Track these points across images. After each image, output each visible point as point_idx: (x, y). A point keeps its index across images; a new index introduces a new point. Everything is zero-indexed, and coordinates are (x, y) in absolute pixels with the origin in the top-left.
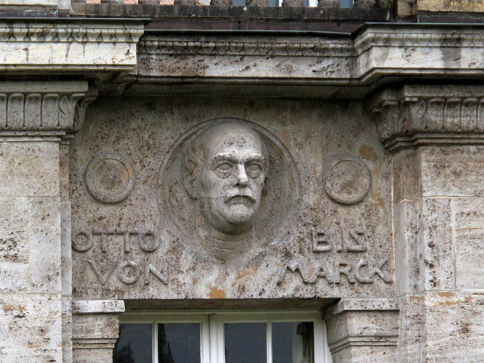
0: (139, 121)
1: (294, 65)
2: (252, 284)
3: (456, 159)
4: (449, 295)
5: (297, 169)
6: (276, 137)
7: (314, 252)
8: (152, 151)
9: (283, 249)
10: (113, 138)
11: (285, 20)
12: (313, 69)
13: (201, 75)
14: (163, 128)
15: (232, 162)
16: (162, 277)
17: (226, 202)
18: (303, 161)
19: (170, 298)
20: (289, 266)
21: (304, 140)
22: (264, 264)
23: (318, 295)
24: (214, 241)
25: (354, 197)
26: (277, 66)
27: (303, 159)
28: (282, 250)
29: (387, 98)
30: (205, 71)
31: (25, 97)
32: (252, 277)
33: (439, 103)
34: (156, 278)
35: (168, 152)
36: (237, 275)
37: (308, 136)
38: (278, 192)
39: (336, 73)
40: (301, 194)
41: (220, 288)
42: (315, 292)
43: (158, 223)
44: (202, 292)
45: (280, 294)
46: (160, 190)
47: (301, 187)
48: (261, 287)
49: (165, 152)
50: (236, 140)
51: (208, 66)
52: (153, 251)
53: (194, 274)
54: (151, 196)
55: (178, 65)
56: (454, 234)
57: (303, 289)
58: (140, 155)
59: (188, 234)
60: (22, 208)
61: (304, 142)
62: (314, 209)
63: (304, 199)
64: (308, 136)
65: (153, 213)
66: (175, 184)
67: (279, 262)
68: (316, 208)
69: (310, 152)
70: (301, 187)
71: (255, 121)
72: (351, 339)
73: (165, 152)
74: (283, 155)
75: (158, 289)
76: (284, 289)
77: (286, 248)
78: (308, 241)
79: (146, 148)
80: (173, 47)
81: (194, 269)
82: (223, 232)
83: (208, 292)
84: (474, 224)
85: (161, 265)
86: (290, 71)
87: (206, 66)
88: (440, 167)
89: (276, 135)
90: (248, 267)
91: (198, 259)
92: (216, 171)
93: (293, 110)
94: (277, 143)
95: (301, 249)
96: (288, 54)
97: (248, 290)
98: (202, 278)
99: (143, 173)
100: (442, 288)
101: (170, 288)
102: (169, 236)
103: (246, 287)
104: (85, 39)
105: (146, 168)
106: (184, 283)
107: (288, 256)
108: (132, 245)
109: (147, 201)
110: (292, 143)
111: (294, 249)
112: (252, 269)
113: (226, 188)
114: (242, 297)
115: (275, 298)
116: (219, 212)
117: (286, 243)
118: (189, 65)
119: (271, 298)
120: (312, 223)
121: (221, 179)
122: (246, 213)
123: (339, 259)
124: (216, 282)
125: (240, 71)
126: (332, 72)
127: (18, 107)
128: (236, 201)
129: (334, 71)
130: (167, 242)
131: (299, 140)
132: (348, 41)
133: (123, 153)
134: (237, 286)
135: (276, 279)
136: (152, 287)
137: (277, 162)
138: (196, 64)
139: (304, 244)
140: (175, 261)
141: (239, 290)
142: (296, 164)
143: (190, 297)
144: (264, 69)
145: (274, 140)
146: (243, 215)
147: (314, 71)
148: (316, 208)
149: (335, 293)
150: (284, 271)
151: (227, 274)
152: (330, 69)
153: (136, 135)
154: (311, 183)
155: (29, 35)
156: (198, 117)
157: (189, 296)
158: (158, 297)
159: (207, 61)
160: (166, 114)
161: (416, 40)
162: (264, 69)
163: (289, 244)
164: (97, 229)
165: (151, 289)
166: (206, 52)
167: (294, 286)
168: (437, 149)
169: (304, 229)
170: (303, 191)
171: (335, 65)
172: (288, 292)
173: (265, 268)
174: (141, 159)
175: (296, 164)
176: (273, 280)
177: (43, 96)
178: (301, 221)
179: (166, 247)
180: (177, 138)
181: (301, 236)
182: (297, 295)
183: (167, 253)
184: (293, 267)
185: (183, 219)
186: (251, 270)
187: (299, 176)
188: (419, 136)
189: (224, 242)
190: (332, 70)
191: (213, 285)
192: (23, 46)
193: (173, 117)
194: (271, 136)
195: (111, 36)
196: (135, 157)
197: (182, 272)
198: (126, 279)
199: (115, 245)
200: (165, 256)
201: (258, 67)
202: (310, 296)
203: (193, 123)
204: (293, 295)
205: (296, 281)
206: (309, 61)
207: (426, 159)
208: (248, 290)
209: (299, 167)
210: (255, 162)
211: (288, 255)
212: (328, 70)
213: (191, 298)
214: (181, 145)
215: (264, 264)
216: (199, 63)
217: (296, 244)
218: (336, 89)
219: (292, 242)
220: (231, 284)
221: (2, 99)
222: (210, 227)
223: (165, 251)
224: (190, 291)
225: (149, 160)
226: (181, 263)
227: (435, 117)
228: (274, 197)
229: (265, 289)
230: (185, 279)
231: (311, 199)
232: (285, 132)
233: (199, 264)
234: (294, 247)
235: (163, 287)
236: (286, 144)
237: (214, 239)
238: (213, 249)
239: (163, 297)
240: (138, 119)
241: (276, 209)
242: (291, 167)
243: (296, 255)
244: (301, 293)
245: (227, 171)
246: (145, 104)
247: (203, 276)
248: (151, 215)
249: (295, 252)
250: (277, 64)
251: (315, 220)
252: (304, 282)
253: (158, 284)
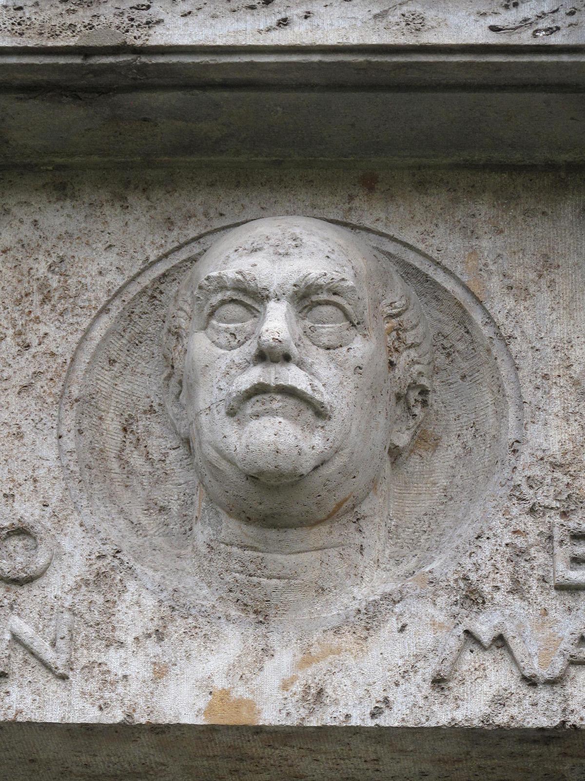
0: (23, 228)
1: (430, 14)
2: (349, 683)
5: (510, 356)
6: (445, 270)
7: (561, 588)
8: (54, 306)
9: (456, 580)
12: (492, 23)
13: (138, 43)
14: (94, 246)
15: (250, 297)
16: (49, 655)
17: (232, 413)
18: (530, 332)
19: (75, 718)
20: (472, 629)
21: (532, 276)
22: (393, 624)
23: (573, 719)
24: (229, 554)
26: (376, 17)
27: (529, 327)
28: (452, 583)
30: (151, 32)
32: (350, 661)
34: (33, 661)
35: (105, 310)
36: (300, 656)
38: (468, 435)
39: (563, 31)
40: (522, 426)
41: (240, 692)
42: (564, 710)
43: (54, 502)
45: (442, 715)
46: (72, 414)
47: (521, 404)
48: (378, 693)
49: (95, 308)
50: (272, 242)
51: (163, 21)
52: (30, 580)
53: (159, 650)
54: (39, 426)
55: (69, 19)
57: (520, 701)
58: (16, 315)
59: (166, 546)
61: (533, 281)
62: (561, 466)
63: (529, 437)
65: (42, 472)
66: (145, 412)
67: (441, 617)
68: (570, 464)
69: (553, 309)
70: (521, 404)
71: (380, 227)
73: (95, 308)
74: (470, 319)
75: (37, 692)
76: (456, 699)
77: (465, 579)
78: (542, 558)
79: (37, 298)
81: (160, 635)
82: (248, 520)
83: (202, 704)
85: (53, 622)
86: (418, 30)
87: (154, 20)
89: (445, 262)
90: (337, 631)
91: (175, 606)
92: (209, 330)
93: (505, 198)
94: (449, 285)
95: (516, 581)
97: (336, 702)
98: (182, 663)
99: (23, 364)
101: (76, 690)
102: (87, 540)
103: (329, 691)
105: (33, 350)
106: (125, 677)
107: (475, 602)
109: (25, 440)
110: (495, 284)
111: (494, 580)
112: (350, 637)
113: (233, 372)
114: (314, 722)
115: (426, 725)
116: (219, 451)
117: (468, 563)
118: (102, 18)
119: (410, 724)
120: (554, 504)
121: (222, 351)
122: (291, 441)
124: (228, 675)
125: (260, 32)
126: (550, 31)
128: (258, 408)
129: (558, 28)
130: (77, 557)
131: (518, 274)
134: (297, 688)
135: (428, 670)
136: (20, 686)
137: (460, 346)
138: (127, 15)
139: (528, 565)
140: (102, 613)
141: (304, 699)
142: (506, 340)
143: (141, 718)
144: (336, 24)
145: (440, 277)
146: (281, 447)
147: (494, 29)
148: (570, 464)
150: (454, 643)
151: (267, 652)
152: (545, 24)
153: (9, 265)
154: (553, 391)
156: (202, 217)
157: (136, 716)
158: (37, 717)
160: (107, 210)
163: (477, 567)
165: (14, 690)
167: (493, 691)
169: (529, 524)
170: (529, 411)
171: (562, 12)
173: (397, 635)
174: (19, 327)
175: (506, 340)
176: (421, 671)
178: (519, 499)
179: (76, 571)
180: (135, 271)
181: (520, 542)
182: (501, 719)
183: (78, 587)
184: (484, 629)
185: (162, 509)
186: (347, 640)
187: (516, 375)
189: (256, 554)
190: (553, 26)
191: (220, 683)
193: (128, 217)
194: (432, 268)
197: (121, 644)
200: (69, 597)
201: (315, 20)
202: (545, 722)
203: (186, 232)
204: (486, 719)
205: (499, 676)
208: (336, 702)
209: (514, 347)
210: (324, 297)
211: (473, 598)
212: (540, 26)
213: (143, 721)
214: (153, 294)
215: (393, 624)
216: (136, 14)
217: (499, 565)
219: (488, 562)
220: (277, 683)
222: (217, 513)
223: (71, 581)
224: (141, 701)
225: (43, 329)
226: (120, 616)
228: (459, 451)
229: (391, 699)
230: (130, 664)
232: (474, 253)
233: (179, 621)
234: (492, 576)
235: (54, 686)
236: (476, 290)
237: (229, 548)
238: (228, 578)
239: (53, 715)
240: (21, 222)
241: (460, 483)
242: (494, 352)
243: (498, 597)
244: (514, 711)
245: (239, 325)
246: (44, 186)
247: (188, 658)
248: (35, 481)
249: (497, 588)
250: (376, 11)
251: (564, 497)
252: (524, 679)
253: (41, 675)
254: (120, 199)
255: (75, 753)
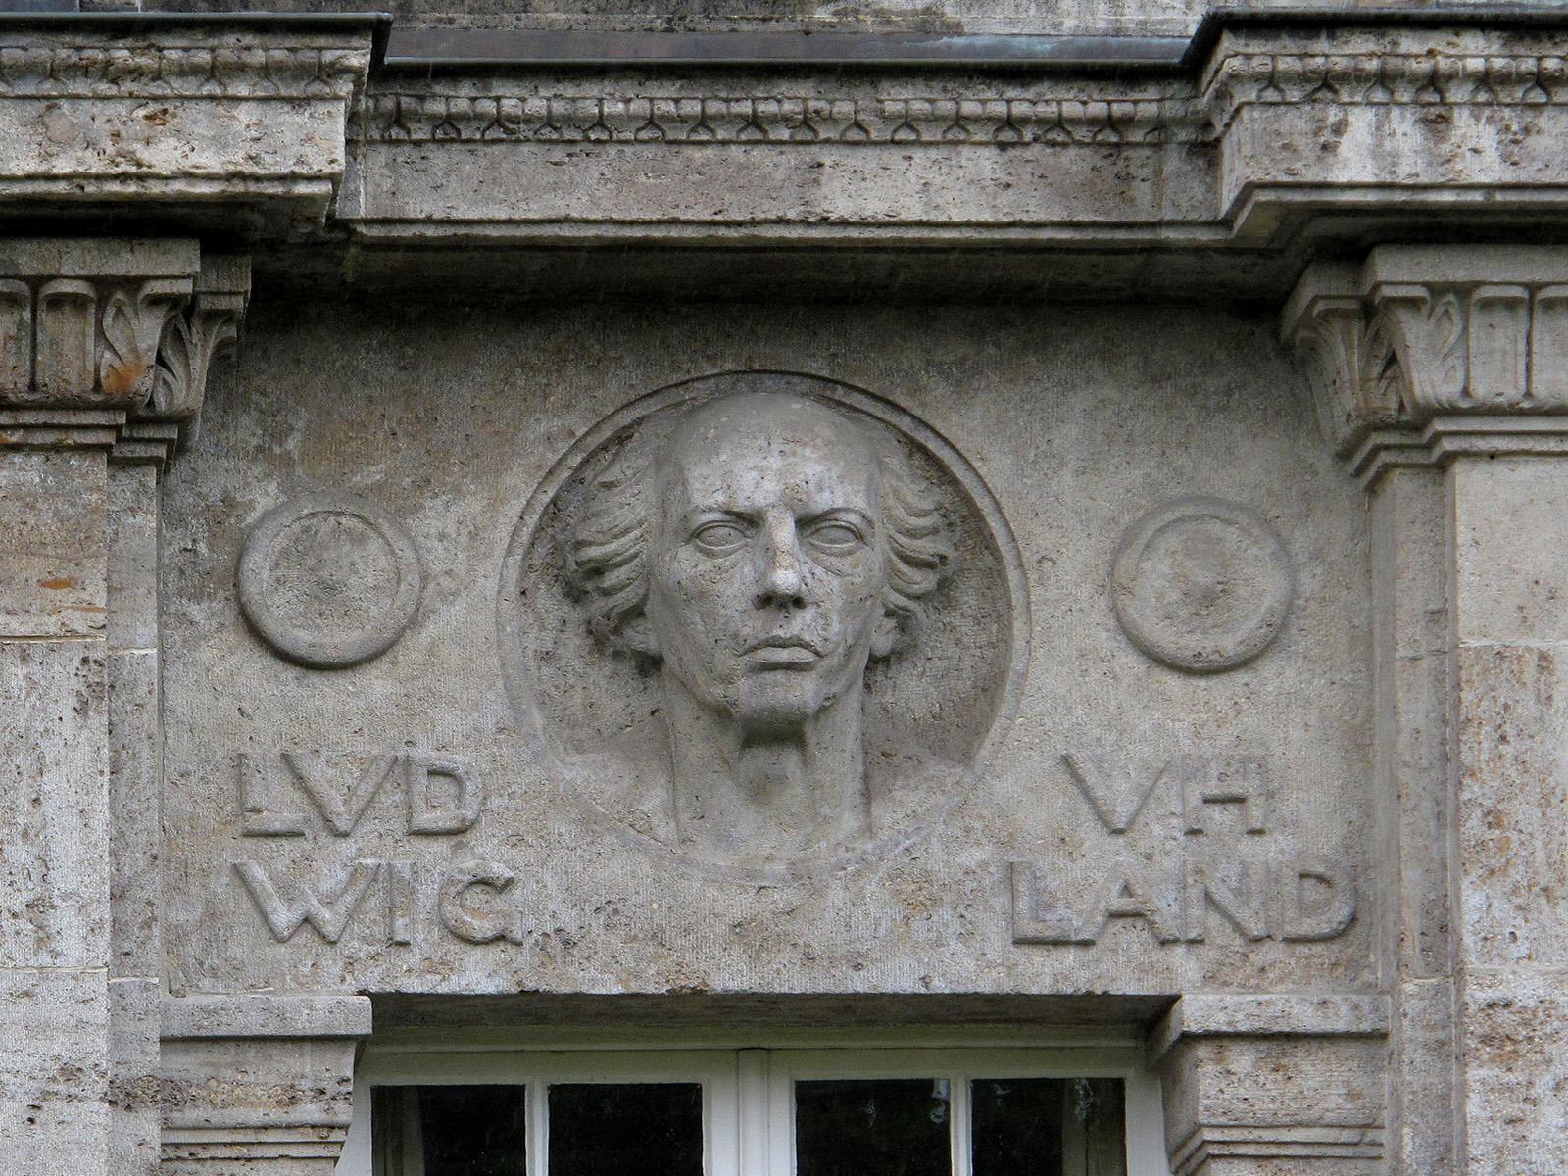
19: (780, 988)
29: (1316, 290)
72: (1208, 1135)
96: (561, 135)
132: (1175, 88)
177: (35, 292)
188: (1439, 426)
218: (1135, 261)
221: (12, 301)
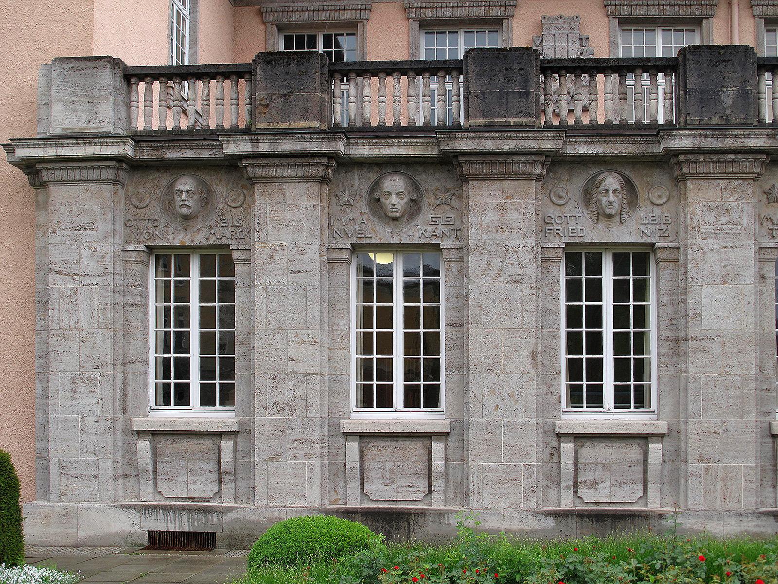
3: (270, 188)
4: (265, 243)
10: (143, 183)
11: (210, 134)
15: (181, 192)
25: (237, 205)
31: (93, 168)
33: (258, 166)
37: (221, 181)
44: (177, 243)
56: (268, 219)
60: (96, 210)
64: (221, 181)
80: (152, 147)
84: (276, 215)
88: (263, 192)
100: (262, 241)
104: (62, 145)
108: (149, 224)
111: (214, 226)
123: (232, 229)
127: (91, 171)
133: (147, 189)
149: (229, 242)
155: (85, 143)
159: (166, 151)
161: (240, 140)
162: (189, 154)
164: (136, 218)
166: (165, 148)
168: (262, 185)
169: (218, 218)
170: (218, 202)
172: (211, 242)
184: (212, 232)
191: (181, 240)
192: (84, 148)
195: (117, 142)
196: (151, 190)
198: (146, 237)
199: (142, 225)
205: (214, 238)
206: (208, 150)
207: (258, 189)
219: (213, 223)
227: (258, 172)
230: (170, 237)
231: (221, 206)
254: (165, 172)
255: (493, 438)
